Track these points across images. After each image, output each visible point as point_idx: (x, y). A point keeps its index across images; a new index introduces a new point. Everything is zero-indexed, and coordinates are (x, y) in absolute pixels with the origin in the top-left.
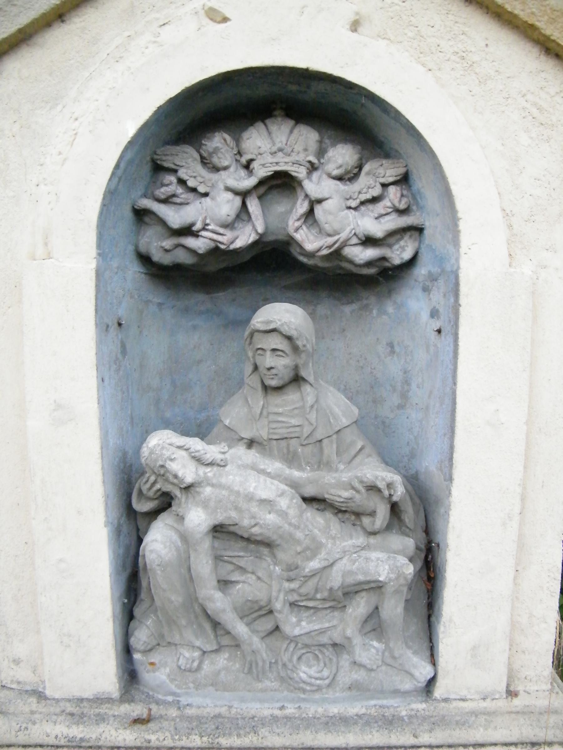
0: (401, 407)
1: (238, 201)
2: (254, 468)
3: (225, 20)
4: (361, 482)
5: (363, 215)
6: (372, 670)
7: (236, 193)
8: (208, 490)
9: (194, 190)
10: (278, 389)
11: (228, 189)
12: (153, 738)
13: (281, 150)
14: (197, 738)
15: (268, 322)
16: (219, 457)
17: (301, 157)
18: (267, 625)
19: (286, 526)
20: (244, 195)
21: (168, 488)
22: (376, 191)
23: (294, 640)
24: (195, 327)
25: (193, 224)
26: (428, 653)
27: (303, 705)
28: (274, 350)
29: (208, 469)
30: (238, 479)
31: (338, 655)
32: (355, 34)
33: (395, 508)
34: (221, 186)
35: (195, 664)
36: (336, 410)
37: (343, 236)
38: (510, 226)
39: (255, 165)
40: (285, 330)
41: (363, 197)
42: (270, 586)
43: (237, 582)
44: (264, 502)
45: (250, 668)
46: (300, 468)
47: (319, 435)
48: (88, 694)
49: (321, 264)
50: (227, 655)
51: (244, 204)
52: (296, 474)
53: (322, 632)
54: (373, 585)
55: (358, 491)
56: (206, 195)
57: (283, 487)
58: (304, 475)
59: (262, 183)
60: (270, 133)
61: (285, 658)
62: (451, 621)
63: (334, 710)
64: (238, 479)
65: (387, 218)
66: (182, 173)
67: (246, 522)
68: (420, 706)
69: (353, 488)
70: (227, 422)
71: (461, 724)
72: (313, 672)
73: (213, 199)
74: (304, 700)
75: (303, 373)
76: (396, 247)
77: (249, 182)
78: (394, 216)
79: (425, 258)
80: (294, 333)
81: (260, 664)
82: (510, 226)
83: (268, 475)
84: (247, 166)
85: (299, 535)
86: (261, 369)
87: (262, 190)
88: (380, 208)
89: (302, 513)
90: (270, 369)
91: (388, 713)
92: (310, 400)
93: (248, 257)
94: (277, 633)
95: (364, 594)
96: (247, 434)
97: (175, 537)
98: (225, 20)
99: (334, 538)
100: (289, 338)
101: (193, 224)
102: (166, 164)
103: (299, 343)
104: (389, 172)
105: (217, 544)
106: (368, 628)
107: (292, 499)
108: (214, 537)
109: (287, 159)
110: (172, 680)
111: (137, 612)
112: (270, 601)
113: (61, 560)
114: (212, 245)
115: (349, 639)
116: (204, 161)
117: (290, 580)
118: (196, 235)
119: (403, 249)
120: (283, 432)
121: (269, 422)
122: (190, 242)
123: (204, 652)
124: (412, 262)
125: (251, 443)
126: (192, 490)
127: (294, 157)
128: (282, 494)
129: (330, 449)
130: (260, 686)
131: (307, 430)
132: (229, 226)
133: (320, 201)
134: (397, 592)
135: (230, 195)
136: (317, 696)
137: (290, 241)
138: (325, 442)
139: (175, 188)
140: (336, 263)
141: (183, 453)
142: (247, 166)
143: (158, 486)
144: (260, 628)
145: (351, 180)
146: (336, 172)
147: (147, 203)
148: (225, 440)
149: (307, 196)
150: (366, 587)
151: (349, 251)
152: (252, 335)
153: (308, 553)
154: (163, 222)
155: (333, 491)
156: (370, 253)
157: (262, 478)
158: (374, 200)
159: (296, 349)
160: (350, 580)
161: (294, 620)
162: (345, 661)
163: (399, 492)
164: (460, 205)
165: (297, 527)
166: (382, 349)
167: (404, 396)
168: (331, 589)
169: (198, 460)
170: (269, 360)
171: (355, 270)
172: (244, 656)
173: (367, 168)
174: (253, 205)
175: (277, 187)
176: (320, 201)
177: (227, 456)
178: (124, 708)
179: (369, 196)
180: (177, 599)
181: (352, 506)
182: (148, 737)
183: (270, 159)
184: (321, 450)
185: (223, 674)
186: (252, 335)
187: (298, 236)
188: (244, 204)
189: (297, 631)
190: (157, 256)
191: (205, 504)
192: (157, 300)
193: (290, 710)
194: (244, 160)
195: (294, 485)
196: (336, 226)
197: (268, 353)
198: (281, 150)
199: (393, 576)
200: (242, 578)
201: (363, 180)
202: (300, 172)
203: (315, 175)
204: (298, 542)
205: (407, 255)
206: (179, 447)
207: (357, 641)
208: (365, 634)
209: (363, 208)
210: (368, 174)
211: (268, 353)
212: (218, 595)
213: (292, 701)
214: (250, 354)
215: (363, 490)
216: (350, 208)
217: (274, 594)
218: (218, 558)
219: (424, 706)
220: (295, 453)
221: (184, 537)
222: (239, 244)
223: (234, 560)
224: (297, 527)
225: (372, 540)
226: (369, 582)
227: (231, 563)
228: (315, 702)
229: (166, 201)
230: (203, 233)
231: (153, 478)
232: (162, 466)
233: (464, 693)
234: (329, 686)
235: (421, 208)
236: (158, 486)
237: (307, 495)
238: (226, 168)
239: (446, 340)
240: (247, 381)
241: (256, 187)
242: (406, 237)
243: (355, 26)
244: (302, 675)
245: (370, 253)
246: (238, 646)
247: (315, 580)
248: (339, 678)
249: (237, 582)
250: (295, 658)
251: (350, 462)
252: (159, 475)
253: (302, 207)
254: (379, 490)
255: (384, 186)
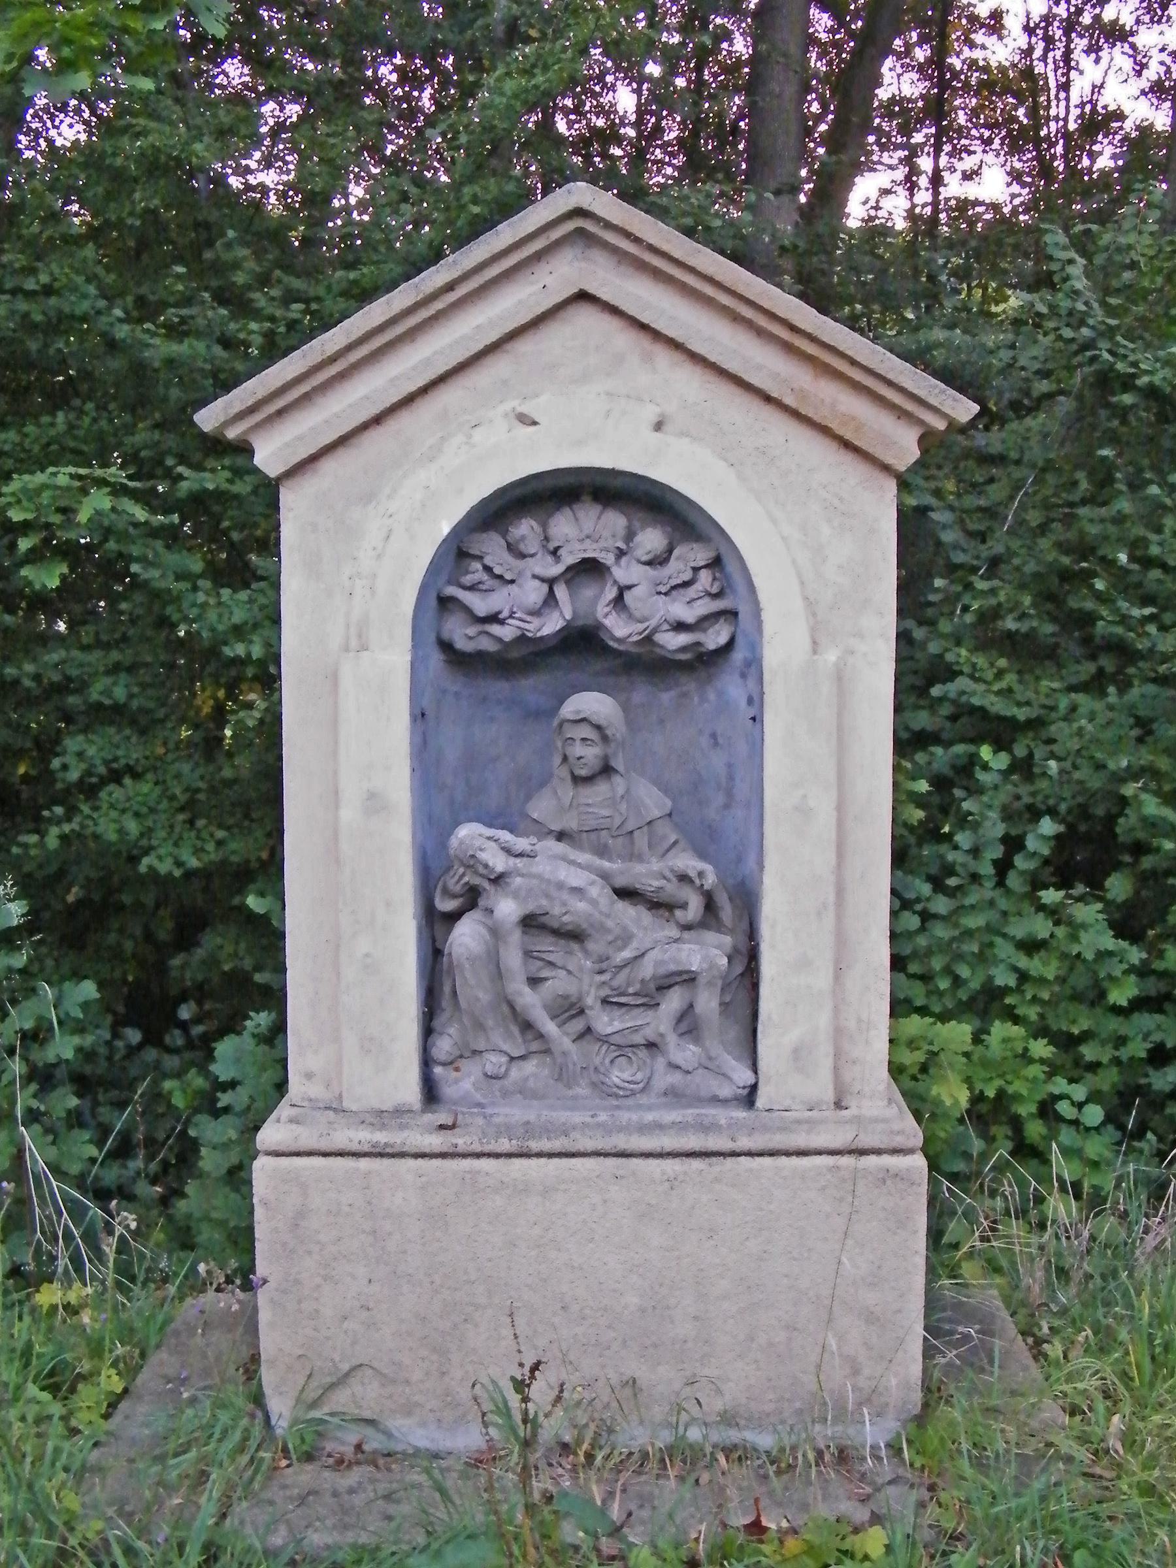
0: (727, 806)
1: (545, 588)
2: (564, 859)
3: (535, 423)
4: (672, 871)
5: (674, 600)
6: (688, 1072)
7: (543, 580)
8: (518, 881)
9: (500, 577)
10: (588, 780)
11: (535, 577)
12: (460, 1141)
13: (588, 537)
14: (506, 1141)
15: (578, 712)
16: (529, 848)
17: (610, 543)
18: (578, 1025)
19: (597, 914)
20: (551, 582)
21: (476, 881)
22: (687, 576)
23: (604, 1040)
24: (492, 719)
25: (500, 612)
26: (750, 1062)
27: (616, 1113)
28: (583, 739)
29: (518, 860)
30: (548, 868)
31: (653, 1057)
32: (657, 434)
33: (710, 905)
34: (529, 574)
35: (503, 1069)
36: (648, 801)
37: (653, 623)
38: (814, 615)
39: (561, 552)
40: (595, 719)
41: (674, 582)
42: (580, 980)
43: (546, 979)
44: (577, 891)
45: (560, 1074)
46: (610, 860)
47: (630, 826)
48: (388, 1106)
49: (634, 650)
50: (535, 1062)
51: (551, 590)
52: (606, 864)
53: (636, 1029)
54: (685, 977)
55: (668, 880)
56: (512, 582)
57: (594, 877)
58: (615, 866)
59: (569, 569)
60: (577, 519)
61: (597, 1061)
62: (770, 1018)
63: (649, 1117)
64: (548, 868)
65: (699, 602)
66: (488, 561)
67: (557, 910)
68: (741, 1114)
69: (665, 878)
70: (535, 816)
71: (783, 1129)
72: (626, 1076)
73: (520, 586)
74: (618, 1107)
75: (613, 764)
76: (711, 631)
77: (556, 570)
78: (707, 600)
79: (740, 641)
80: (603, 723)
81: (571, 1066)
82: (814, 615)
83: (579, 865)
84: (555, 552)
85: (610, 923)
86: (571, 759)
87: (569, 576)
88: (692, 592)
89: (613, 903)
90: (580, 758)
91: (706, 1122)
92: (621, 790)
93: (553, 642)
94: (588, 1037)
95: (676, 988)
96: (556, 827)
97: (484, 931)
98: (535, 423)
99: (646, 929)
100: (598, 728)
101: (500, 612)
102: (472, 552)
103: (609, 732)
104: (699, 556)
105: (526, 938)
106: (683, 1027)
107: (603, 888)
108: (524, 933)
109: (595, 546)
110: (477, 1089)
111: (436, 1023)
112: (580, 999)
113: (367, 955)
114: (519, 633)
115: (662, 1035)
116: (512, 548)
117: (601, 972)
118: (502, 622)
119: (718, 633)
120: (593, 824)
121: (580, 814)
122: (495, 629)
123: (512, 1059)
124: (730, 645)
125: (561, 836)
126: (501, 881)
127: (602, 544)
128: (593, 883)
129: (641, 840)
130: (570, 1093)
131: (617, 821)
132: (536, 613)
133: (629, 587)
134: (710, 984)
135: (537, 583)
136: (630, 1102)
137: (599, 626)
138: (636, 834)
139: (482, 576)
140: (648, 648)
141: (493, 844)
142: (555, 552)
143: (466, 879)
144: (570, 1030)
145: (661, 564)
146: (645, 558)
147: (452, 591)
148: (534, 834)
149: (615, 582)
150: (678, 979)
151: (661, 638)
152: (561, 725)
153: (619, 943)
154: (468, 610)
155: (643, 881)
156: (683, 639)
157: (572, 868)
158: (686, 584)
159: (605, 739)
160: (662, 971)
161: (606, 1019)
162: (660, 1063)
163: (710, 880)
164: (762, 596)
165: (608, 916)
166: (705, 741)
167: (729, 794)
168: (643, 981)
169: (508, 851)
170: (578, 750)
171: (669, 656)
172: (554, 1059)
173: (676, 553)
174: (561, 592)
175: (585, 571)
176: (629, 587)
177: (537, 847)
178: (429, 1118)
179: (679, 581)
180: (485, 997)
181: (663, 897)
182: (454, 1141)
183: (578, 546)
184: (632, 843)
185: (531, 1080)
186: (561, 725)
187: (607, 622)
188: (551, 590)
189: (609, 1030)
190: (461, 644)
191: (516, 895)
192: (454, 688)
193: (603, 1117)
194: (551, 546)
195: (605, 876)
196: (646, 613)
197: (578, 742)
198: (588, 537)
199: (705, 966)
200: (553, 974)
201: (674, 565)
202: (608, 559)
203: (624, 560)
204: (609, 931)
205: (723, 639)
206: (489, 838)
207: (672, 1039)
208: (682, 1034)
209: (674, 593)
210: (678, 559)
211: (578, 742)
212: (527, 990)
213: (605, 1109)
214: (559, 744)
215: (674, 880)
216: (659, 593)
217: (585, 988)
218: (528, 954)
219: (744, 1114)
220: (606, 846)
221: (495, 932)
222: (546, 631)
223: (544, 956)
224: (608, 916)
225: (687, 935)
226: (680, 973)
227: (542, 960)
228: (629, 1109)
229: (471, 588)
230: (510, 621)
231: (461, 870)
232: (473, 856)
233: (787, 1103)
234: (643, 1090)
235: (734, 591)
236: (466, 879)
237: (617, 886)
238: (532, 556)
239: (758, 725)
240: (556, 772)
241: (563, 574)
242: (722, 620)
243: (658, 426)
244: (616, 1080)
245: (683, 639)
246: (547, 1052)
247: (626, 971)
248: (654, 1082)
249: (546, 979)
250: (607, 1061)
251: (664, 855)
252: (468, 867)
253: (611, 593)
254: (691, 881)
255: (696, 570)
